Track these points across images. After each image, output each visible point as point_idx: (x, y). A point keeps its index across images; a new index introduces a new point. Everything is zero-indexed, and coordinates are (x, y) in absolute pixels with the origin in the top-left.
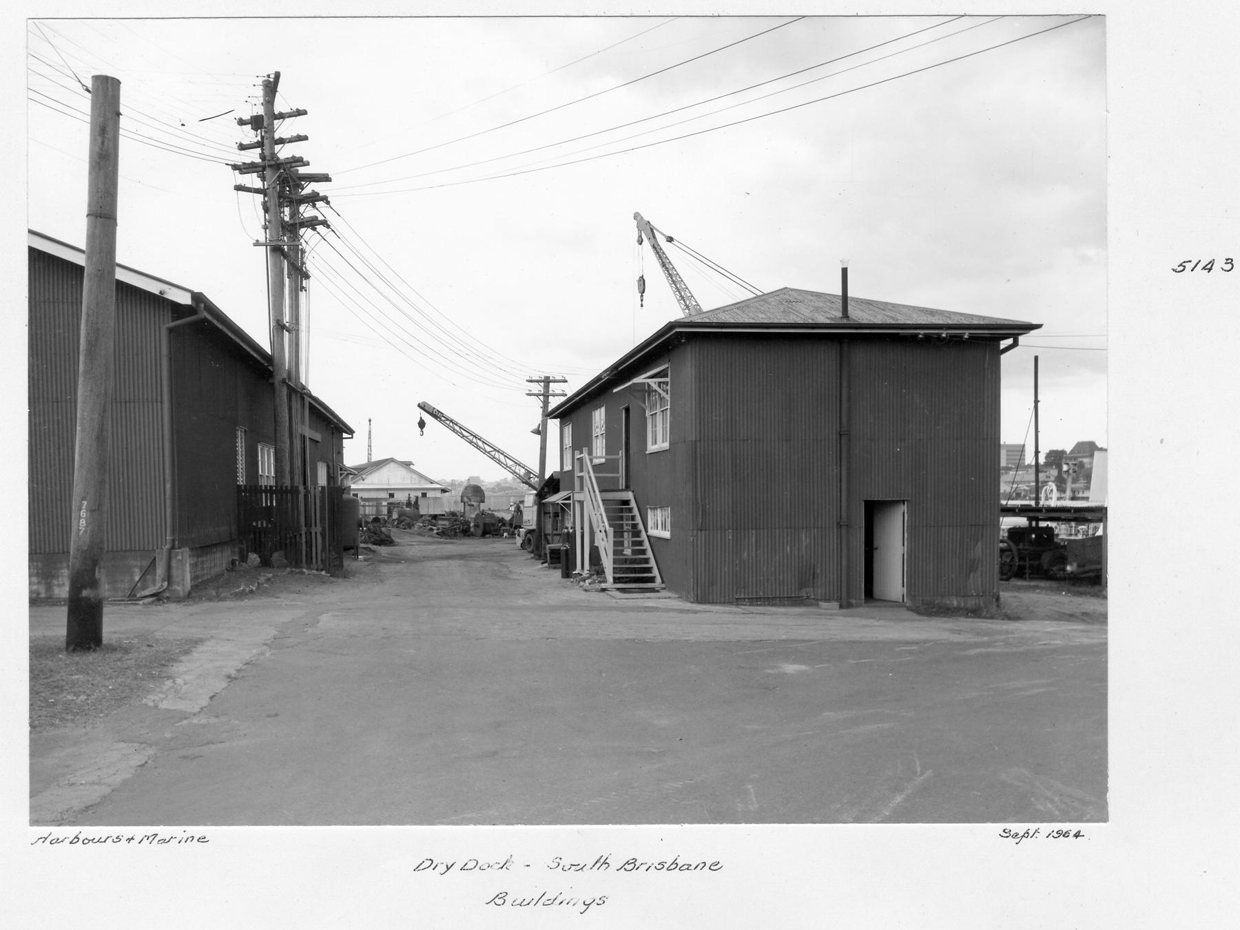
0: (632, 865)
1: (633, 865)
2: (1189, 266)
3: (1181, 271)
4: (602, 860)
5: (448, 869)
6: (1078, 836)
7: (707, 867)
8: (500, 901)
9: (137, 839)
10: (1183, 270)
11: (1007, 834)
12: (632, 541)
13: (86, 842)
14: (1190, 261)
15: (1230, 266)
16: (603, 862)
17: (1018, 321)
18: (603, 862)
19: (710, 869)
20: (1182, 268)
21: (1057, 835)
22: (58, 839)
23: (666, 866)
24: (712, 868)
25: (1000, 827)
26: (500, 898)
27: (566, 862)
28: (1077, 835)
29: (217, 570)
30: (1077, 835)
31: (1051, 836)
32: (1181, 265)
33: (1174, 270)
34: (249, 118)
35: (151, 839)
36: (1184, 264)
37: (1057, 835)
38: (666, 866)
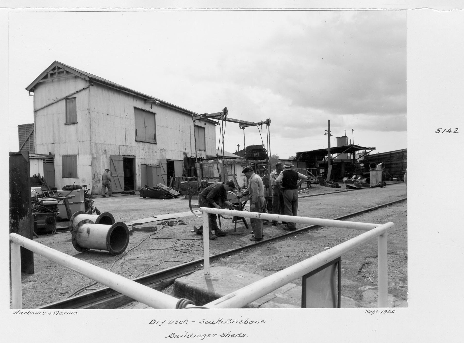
0: (33, 313)
1: (230, 322)
2: (441, 131)
3: (439, 132)
4: (220, 320)
5: (163, 323)
6: (394, 312)
7: (73, 313)
8: (228, 322)
9: (52, 313)
10: (440, 132)
11: (367, 312)
12: (46, 197)
13: (177, 322)
14: (441, 129)
15: (439, 131)
16: (220, 321)
17: (119, 85)
18: (220, 321)
19: (74, 314)
20: (438, 131)
21: (385, 312)
22: (22, 313)
23: (244, 322)
24: (232, 336)
25: (365, 309)
26: (172, 336)
27: (249, 321)
28: (393, 312)
29: (167, 246)
30: (393, 312)
31: (382, 312)
32: (438, 130)
33: (436, 132)
34: (295, 155)
35: (57, 313)
36: (439, 130)
37: (385, 312)
38: (244, 322)
